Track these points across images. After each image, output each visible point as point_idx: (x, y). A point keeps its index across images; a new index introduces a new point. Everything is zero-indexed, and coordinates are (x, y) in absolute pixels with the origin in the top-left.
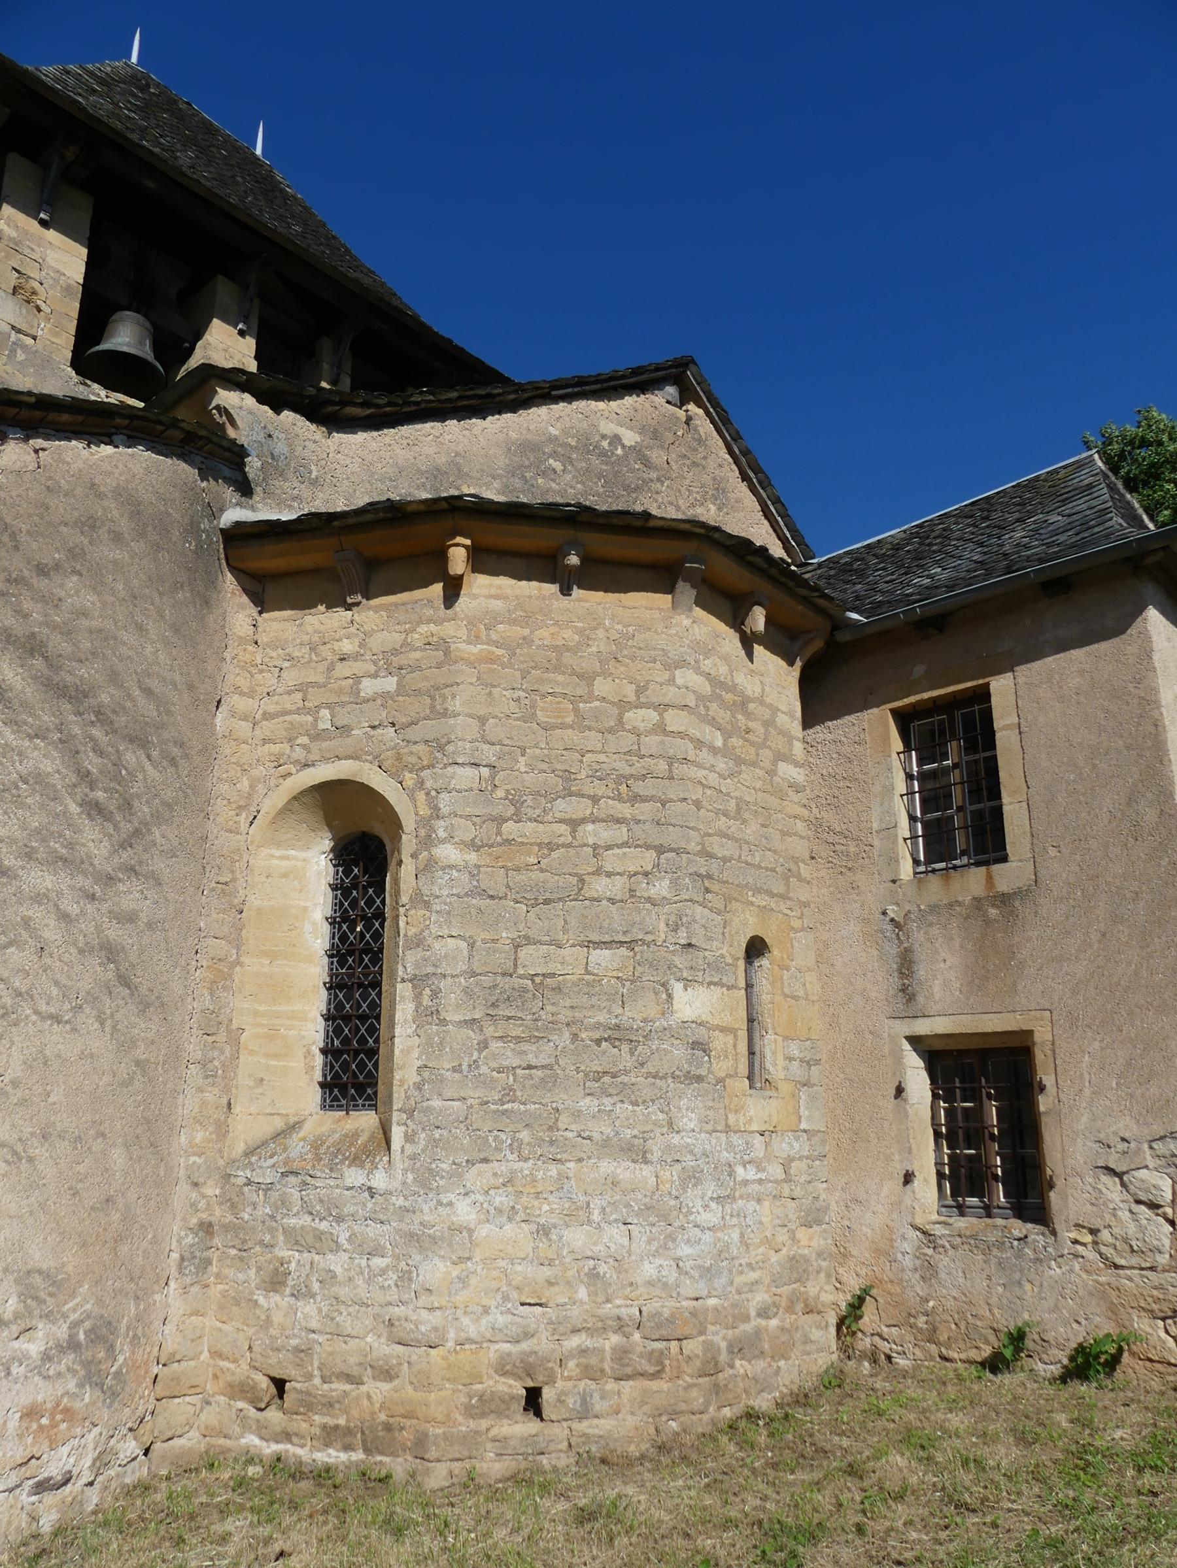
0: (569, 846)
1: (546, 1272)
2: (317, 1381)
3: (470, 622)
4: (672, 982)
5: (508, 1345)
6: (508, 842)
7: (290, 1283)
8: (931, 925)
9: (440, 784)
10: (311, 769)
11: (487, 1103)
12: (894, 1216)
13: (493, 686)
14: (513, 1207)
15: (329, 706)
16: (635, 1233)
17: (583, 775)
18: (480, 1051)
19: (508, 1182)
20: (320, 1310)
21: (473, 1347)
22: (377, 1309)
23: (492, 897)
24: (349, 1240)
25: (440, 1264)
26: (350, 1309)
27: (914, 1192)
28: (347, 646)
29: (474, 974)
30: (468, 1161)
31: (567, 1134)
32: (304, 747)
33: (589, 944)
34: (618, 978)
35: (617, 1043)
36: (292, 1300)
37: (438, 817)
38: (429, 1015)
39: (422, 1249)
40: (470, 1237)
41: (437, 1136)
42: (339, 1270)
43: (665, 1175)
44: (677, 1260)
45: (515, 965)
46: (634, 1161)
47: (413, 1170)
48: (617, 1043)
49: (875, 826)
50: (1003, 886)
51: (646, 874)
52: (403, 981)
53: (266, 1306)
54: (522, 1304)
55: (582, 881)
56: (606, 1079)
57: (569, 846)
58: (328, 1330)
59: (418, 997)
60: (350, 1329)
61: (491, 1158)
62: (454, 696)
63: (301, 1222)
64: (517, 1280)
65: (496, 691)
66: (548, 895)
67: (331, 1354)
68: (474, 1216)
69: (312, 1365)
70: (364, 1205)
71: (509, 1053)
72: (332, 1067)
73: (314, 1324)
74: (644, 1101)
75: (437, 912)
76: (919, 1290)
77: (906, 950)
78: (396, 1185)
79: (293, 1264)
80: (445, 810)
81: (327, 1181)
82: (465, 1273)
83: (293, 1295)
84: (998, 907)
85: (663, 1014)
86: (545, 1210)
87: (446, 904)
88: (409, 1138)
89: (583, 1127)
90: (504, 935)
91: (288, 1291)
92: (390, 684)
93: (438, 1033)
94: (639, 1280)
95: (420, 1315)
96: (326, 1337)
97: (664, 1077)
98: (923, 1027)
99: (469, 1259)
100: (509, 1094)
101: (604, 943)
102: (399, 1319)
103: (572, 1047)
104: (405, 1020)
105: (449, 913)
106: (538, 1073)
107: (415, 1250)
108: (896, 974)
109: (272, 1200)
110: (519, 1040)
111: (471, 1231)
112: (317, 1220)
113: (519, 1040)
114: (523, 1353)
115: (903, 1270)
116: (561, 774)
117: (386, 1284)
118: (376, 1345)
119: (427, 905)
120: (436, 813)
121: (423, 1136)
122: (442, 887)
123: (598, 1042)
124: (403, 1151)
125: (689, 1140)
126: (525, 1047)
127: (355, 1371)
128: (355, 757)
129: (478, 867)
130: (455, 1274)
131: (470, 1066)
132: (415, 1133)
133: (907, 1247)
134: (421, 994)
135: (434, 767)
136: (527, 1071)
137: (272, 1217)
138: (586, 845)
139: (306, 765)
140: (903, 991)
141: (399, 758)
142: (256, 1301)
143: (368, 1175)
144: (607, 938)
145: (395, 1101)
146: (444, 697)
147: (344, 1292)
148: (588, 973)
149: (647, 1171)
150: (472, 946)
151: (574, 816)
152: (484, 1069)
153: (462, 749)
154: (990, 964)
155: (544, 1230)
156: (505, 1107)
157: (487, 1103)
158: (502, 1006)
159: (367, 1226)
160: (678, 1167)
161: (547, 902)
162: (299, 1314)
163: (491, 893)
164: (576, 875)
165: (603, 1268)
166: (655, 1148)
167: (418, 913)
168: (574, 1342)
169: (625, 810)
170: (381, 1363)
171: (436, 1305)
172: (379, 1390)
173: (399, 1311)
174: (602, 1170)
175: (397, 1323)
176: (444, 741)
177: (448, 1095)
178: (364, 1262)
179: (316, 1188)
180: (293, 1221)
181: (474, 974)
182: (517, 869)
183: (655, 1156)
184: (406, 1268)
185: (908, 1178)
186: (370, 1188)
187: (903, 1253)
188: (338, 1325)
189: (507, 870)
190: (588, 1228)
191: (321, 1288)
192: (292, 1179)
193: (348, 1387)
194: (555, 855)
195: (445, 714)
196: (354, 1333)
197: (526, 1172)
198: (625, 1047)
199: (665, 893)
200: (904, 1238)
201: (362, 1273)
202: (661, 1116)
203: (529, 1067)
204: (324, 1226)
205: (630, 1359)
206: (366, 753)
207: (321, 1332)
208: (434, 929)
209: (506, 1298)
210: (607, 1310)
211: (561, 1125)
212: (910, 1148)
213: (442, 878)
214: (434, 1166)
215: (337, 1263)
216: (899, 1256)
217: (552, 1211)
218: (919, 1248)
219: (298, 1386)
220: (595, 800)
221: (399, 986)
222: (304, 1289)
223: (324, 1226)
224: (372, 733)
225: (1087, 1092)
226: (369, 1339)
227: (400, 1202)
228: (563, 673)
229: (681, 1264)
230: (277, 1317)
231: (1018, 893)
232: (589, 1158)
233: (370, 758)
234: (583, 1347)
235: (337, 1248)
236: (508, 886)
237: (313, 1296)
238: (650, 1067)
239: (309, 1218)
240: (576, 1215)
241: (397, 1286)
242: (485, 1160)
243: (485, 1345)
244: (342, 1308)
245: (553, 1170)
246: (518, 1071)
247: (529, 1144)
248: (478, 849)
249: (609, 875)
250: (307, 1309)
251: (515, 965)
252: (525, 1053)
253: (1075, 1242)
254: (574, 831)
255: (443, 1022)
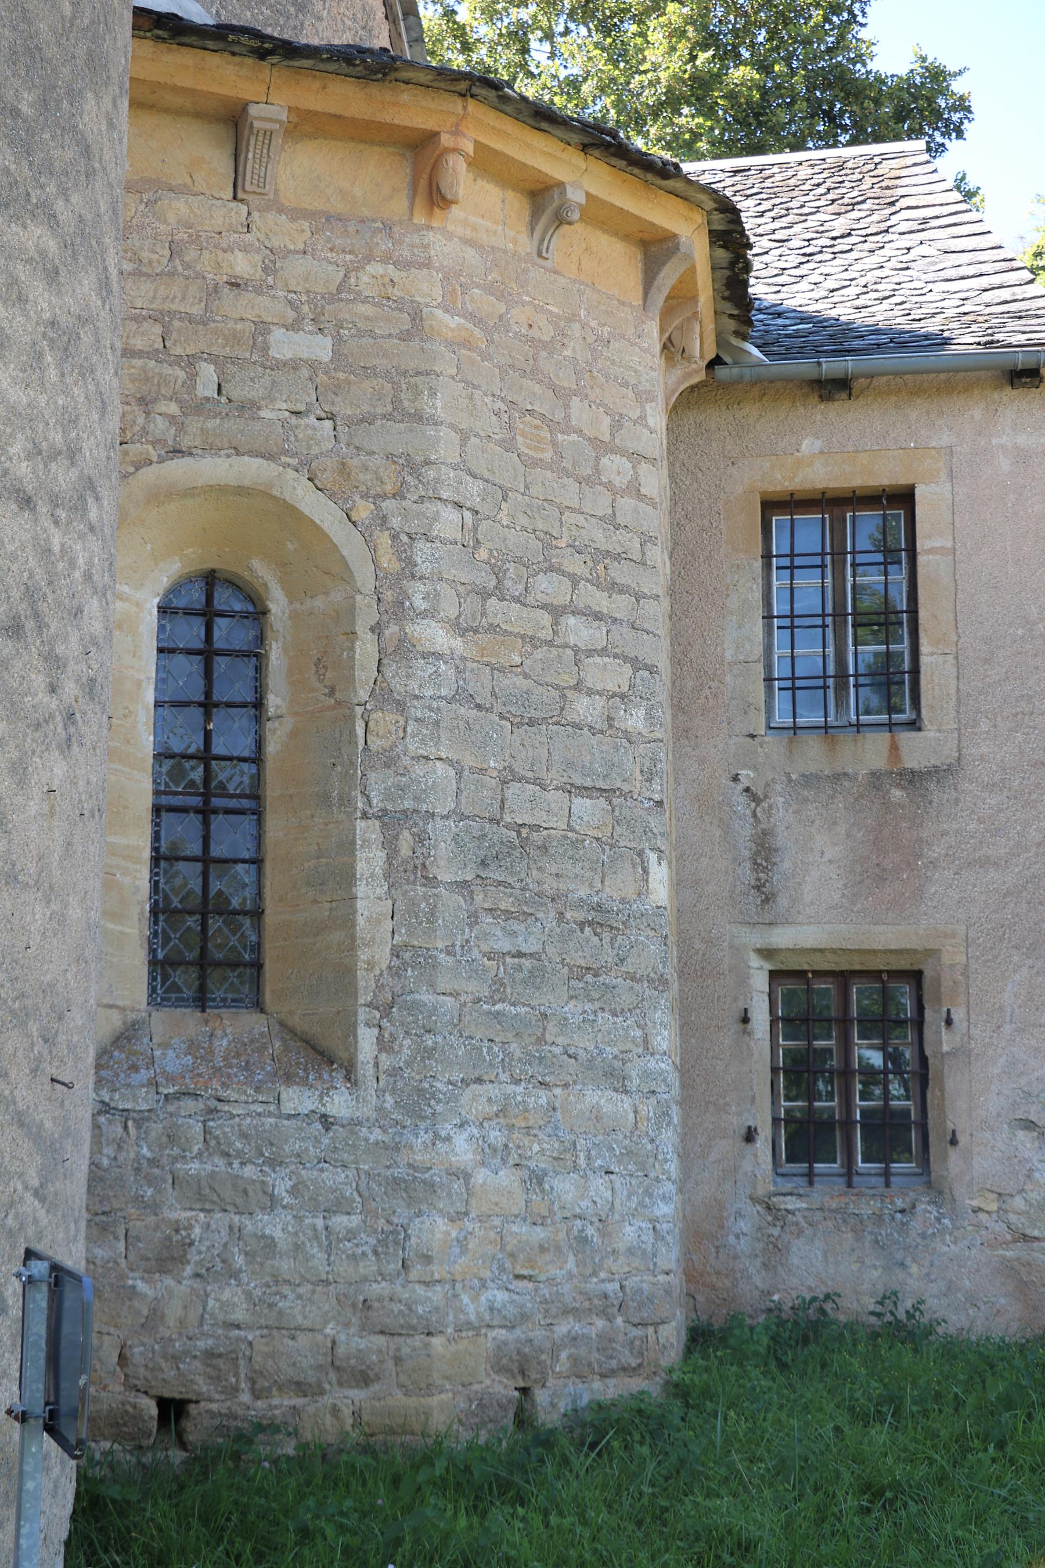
0: (550, 643)
1: (540, 1234)
2: (245, 1397)
3: (446, 278)
4: (647, 851)
5: (503, 1332)
6: (493, 628)
7: (193, 1256)
8: (806, 800)
9: (413, 526)
10: (188, 460)
11: (480, 1000)
12: (728, 1186)
13: (475, 387)
14: (506, 1146)
15: (213, 359)
16: (617, 1185)
17: (562, 543)
18: (471, 926)
19: (502, 1112)
20: (248, 1295)
21: (470, 1333)
22: (341, 1288)
23: (479, 707)
24: (294, 1191)
25: (440, 1221)
26: (301, 1290)
27: (756, 1156)
28: (242, 265)
29: (463, 817)
30: (463, 1080)
31: (554, 1049)
32: (172, 419)
33: (572, 790)
34: (598, 839)
35: (599, 930)
36: (197, 1284)
37: (413, 576)
38: (409, 871)
39: (411, 1201)
40: (467, 1183)
41: (430, 1043)
42: (278, 1234)
43: (643, 1109)
44: (654, 1221)
45: (502, 808)
46: (616, 1090)
47: (393, 1091)
48: (599, 930)
49: (729, 655)
50: (912, 761)
51: (623, 697)
52: (365, 816)
53: (151, 1293)
54: (517, 1277)
55: (563, 696)
56: (589, 978)
57: (550, 643)
58: (263, 1322)
59: (390, 845)
60: (300, 1319)
61: (486, 1078)
62: (433, 394)
63: (209, 1167)
64: (512, 1244)
65: (478, 393)
66: (534, 714)
67: (271, 1355)
68: (471, 1157)
69: (236, 1375)
70: (317, 1141)
71: (499, 933)
72: (167, 939)
73: (239, 1315)
74: (623, 1010)
75: (417, 720)
76: (759, 1284)
77: (765, 833)
78: (367, 1111)
79: (197, 1230)
80: (424, 568)
81: (253, 1107)
82: (463, 1234)
83: (197, 1275)
84: (903, 788)
85: (639, 895)
86: (538, 1150)
87: (431, 709)
88: (384, 1045)
89: (569, 1041)
90: (492, 764)
91: (189, 1270)
92: (322, 348)
93: (425, 897)
94: (621, 1246)
95: (414, 1291)
96: (258, 1333)
97: (640, 981)
98: (782, 938)
99: (466, 1214)
100: (498, 990)
101: (586, 788)
102: (380, 1299)
103: (558, 930)
104: (372, 876)
105: (437, 723)
106: (527, 963)
107: (402, 1203)
108: (748, 865)
109: (153, 1134)
110: (508, 915)
111: (467, 1176)
112: (236, 1164)
113: (508, 915)
114: (518, 1340)
115: (736, 1257)
116: (542, 535)
117: (359, 1251)
118: (343, 1337)
119: (401, 707)
120: (409, 569)
121: (407, 1042)
122: (418, 680)
123: (582, 925)
124: (376, 1065)
125: (663, 1065)
126: (515, 926)
127: (311, 1377)
128: (271, 457)
129: (464, 659)
130: (454, 1234)
131: (463, 947)
132: (393, 1037)
133: (743, 1225)
134: (396, 837)
135: (404, 498)
136: (516, 960)
137: (153, 1162)
138: (566, 646)
139: (177, 452)
140: (758, 888)
141: (343, 468)
142: (134, 1287)
143: (321, 1097)
144: (588, 783)
145: (361, 992)
146: (417, 393)
147: (285, 1266)
148: (572, 830)
149: (625, 1104)
150: (459, 774)
151: (555, 602)
152: (475, 954)
153: (449, 482)
154: (887, 864)
155: (537, 1177)
156: (497, 1007)
157: (480, 1000)
158: (493, 866)
159: (322, 1170)
160: (653, 1100)
161: (532, 723)
162: (211, 1303)
163: (478, 701)
164: (556, 687)
165: (590, 1231)
166: (634, 1074)
167: (385, 720)
168: (563, 1328)
169: (601, 601)
170: (353, 1362)
171: (437, 1276)
172: (351, 1398)
173: (378, 1289)
174: (588, 1099)
175: (376, 1305)
176: (419, 459)
177: (441, 986)
178: (320, 1223)
179: (232, 1116)
180: (194, 1167)
181: (463, 817)
182: (502, 670)
183: (634, 1084)
184: (388, 1228)
185: (750, 1136)
186: (324, 1116)
187: (737, 1237)
188: (280, 1313)
189: (493, 669)
190: (576, 1176)
191: (247, 1263)
192: (190, 1105)
193: (299, 1402)
194: (538, 654)
195: (418, 417)
196: (307, 1324)
197: (519, 1098)
198: (606, 936)
199: (640, 726)
200: (739, 1214)
201: (317, 1238)
202: (639, 1033)
203: (520, 955)
204: (249, 1171)
205: (614, 1349)
206: (286, 452)
207: (250, 1328)
208: (413, 746)
209: (502, 1269)
210: (593, 1286)
211: (549, 1038)
212: (754, 1097)
213: (423, 669)
214: (426, 1085)
215: (275, 1226)
216: (731, 1239)
217: (542, 1152)
218: (759, 1229)
219: (214, 1407)
220: (575, 580)
221: (360, 824)
222: (219, 1265)
223: (249, 1171)
224: (293, 420)
225: (1008, 1029)
226: (328, 1331)
227: (376, 1135)
228: (540, 382)
229: (658, 1226)
230: (173, 1312)
231: (934, 772)
232: (575, 1082)
233: (294, 462)
234: (573, 1333)
235: (272, 1202)
236: (493, 694)
237: (235, 1274)
238: (628, 967)
239: (220, 1162)
240: (564, 1159)
241: (375, 1252)
242: (479, 1080)
243: (483, 1331)
244: (286, 1290)
245: (543, 1097)
246: (508, 960)
247: (520, 1060)
248: (462, 632)
249: (590, 692)
250: (226, 1295)
251: (502, 808)
252: (514, 934)
253: (977, 1210)
254: (556, 623)
255: (431, 882)
